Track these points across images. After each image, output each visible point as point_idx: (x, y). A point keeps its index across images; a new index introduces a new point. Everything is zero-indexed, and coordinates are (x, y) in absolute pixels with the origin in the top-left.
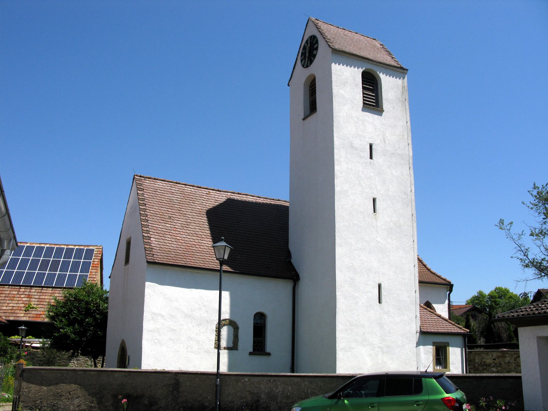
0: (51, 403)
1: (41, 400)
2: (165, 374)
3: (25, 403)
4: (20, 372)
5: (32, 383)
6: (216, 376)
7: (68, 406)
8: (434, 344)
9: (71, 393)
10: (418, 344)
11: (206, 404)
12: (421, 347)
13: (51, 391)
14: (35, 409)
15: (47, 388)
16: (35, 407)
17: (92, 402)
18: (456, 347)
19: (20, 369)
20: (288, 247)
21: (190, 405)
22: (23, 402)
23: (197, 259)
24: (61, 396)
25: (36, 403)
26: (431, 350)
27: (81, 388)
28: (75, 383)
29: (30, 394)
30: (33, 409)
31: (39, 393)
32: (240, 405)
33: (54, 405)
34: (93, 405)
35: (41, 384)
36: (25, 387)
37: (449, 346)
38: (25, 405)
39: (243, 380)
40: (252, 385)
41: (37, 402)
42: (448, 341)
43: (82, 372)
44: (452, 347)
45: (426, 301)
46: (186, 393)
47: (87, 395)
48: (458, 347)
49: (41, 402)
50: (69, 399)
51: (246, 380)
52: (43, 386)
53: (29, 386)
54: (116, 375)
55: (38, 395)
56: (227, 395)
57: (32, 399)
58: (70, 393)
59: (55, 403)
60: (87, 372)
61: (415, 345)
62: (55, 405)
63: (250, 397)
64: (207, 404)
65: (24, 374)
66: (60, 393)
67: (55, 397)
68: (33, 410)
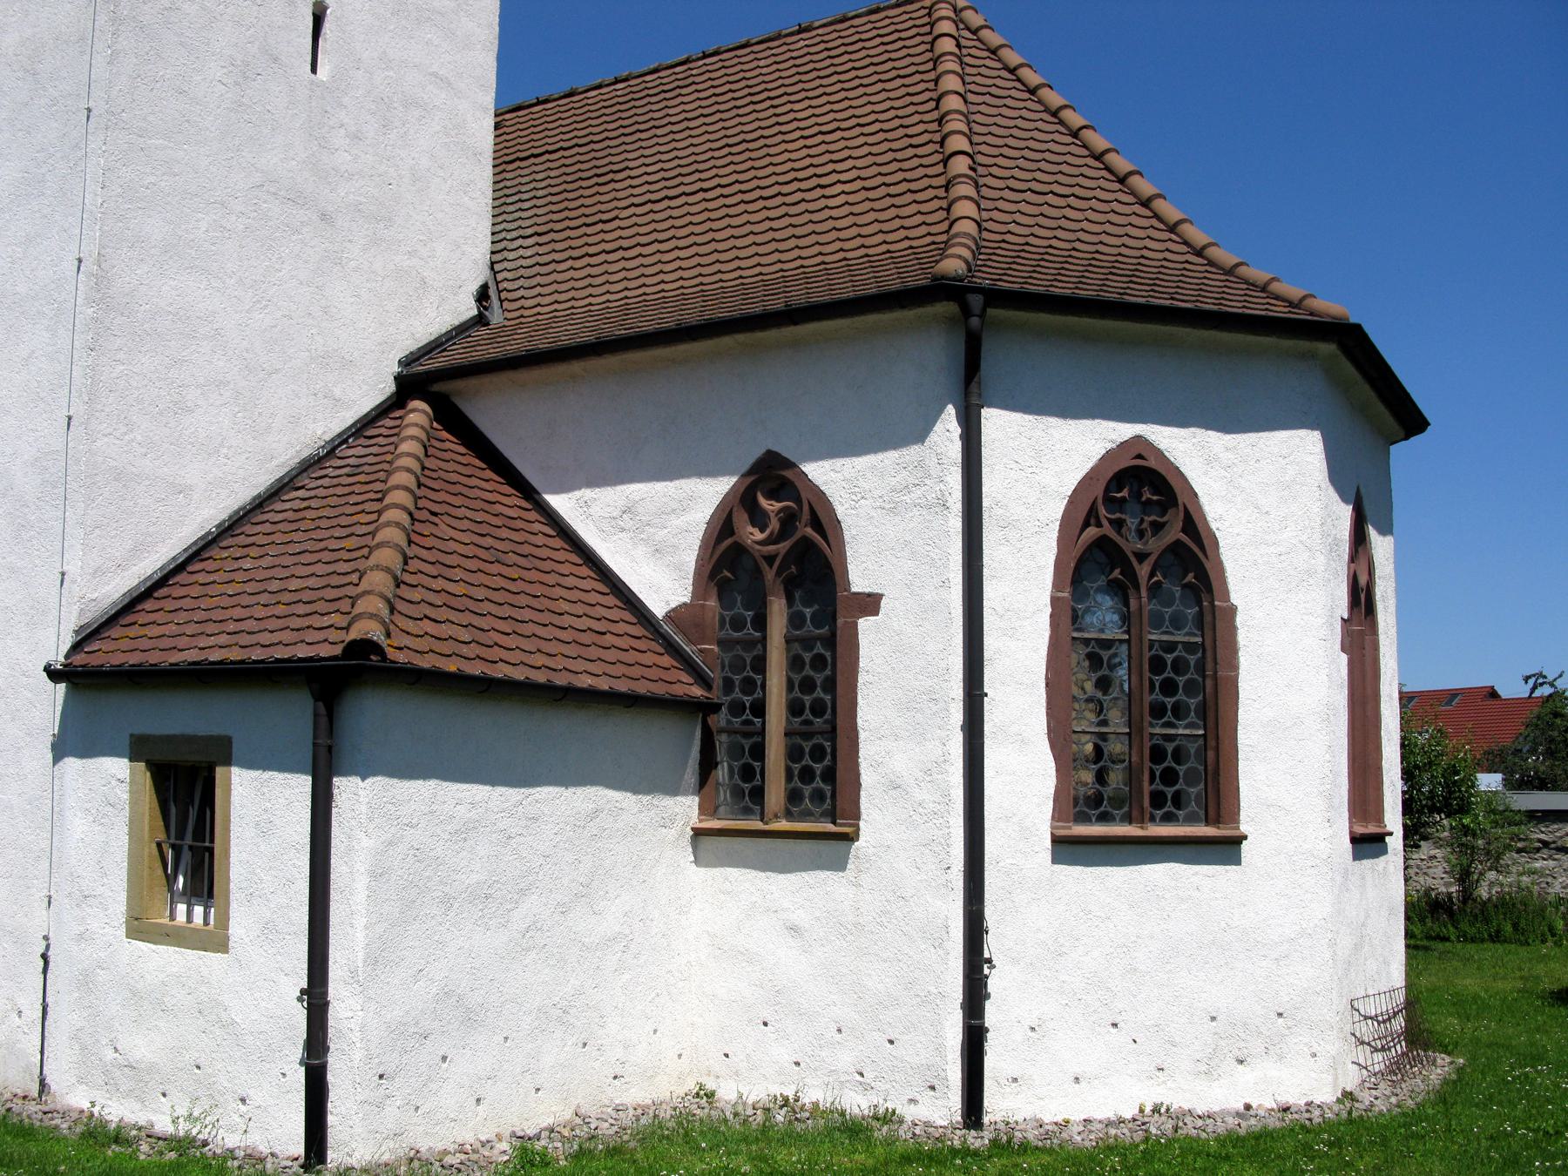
8: (138, 749)
10: (61, 749)
12: (71, 764)
18: (281, 768)
23: (1051, 137)
26: (123, 794)
37: (228, 762)
42: (229, 732)
44: (250, 765)
45: (756, 453)
48: (1406, 980)
61: (50, 756)
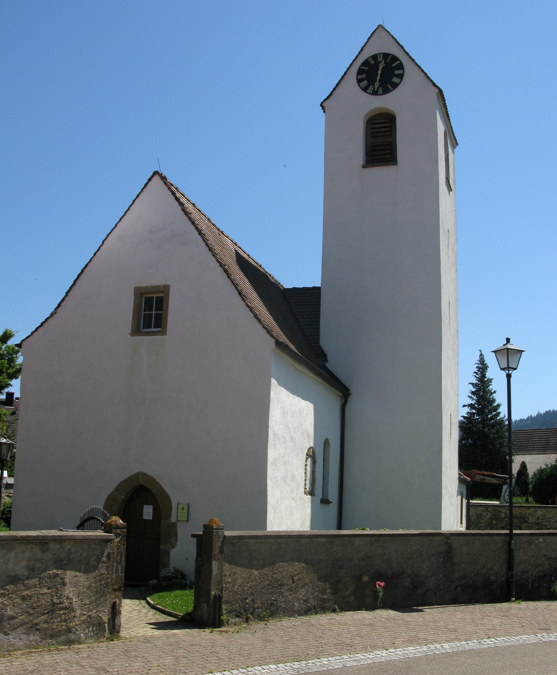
0: (267, 600)
1: (253, 597)
2: (431, 537)
3: (229, 604)
4: (220, 545)
5: (238, 565)
6: (508, 537)
7: (291, 604)
9: (294, 578)
11: (492, 578)
13: (265, 578)
14: (245, 615)
15: (259, 573)
16: (245, 611)
17: (323, 592)
19: (220, 537)
20: (319, 343)
21: (470, 582)
22: (227, 602)
24: (281, 585)
25: (247, 604)
27: (308, 568)
28: (298, 561)
29: (236, 587)
30: (241, 614)
31: (248, 583)
32: (536, 576)
33: (272, 604)
34: (325, 596)
35: (250, 566)
36: (228, 574)
38: (229, 608)
39: (537, 542)
40: (549, 548)
41: (248, 601)
43: (307, 540)
46: (463, 565)
47: (315, 581)
49: (253, 600)
50: (291, 591)
51: (540, 540)
52: (252, 569)
53: (234, 570)
54: (357, 541)
55: (247, 587)
56: (517, 563)
57: (239, 596)
58: (293, 579)
59: (274, 601)
60: (315, 539)
62: (274, 603)
63: (547, 564)
64: (493, 578)
65: (225, 548)
66: (280, 580)
67: (272, 588)
68: (242, 616)
